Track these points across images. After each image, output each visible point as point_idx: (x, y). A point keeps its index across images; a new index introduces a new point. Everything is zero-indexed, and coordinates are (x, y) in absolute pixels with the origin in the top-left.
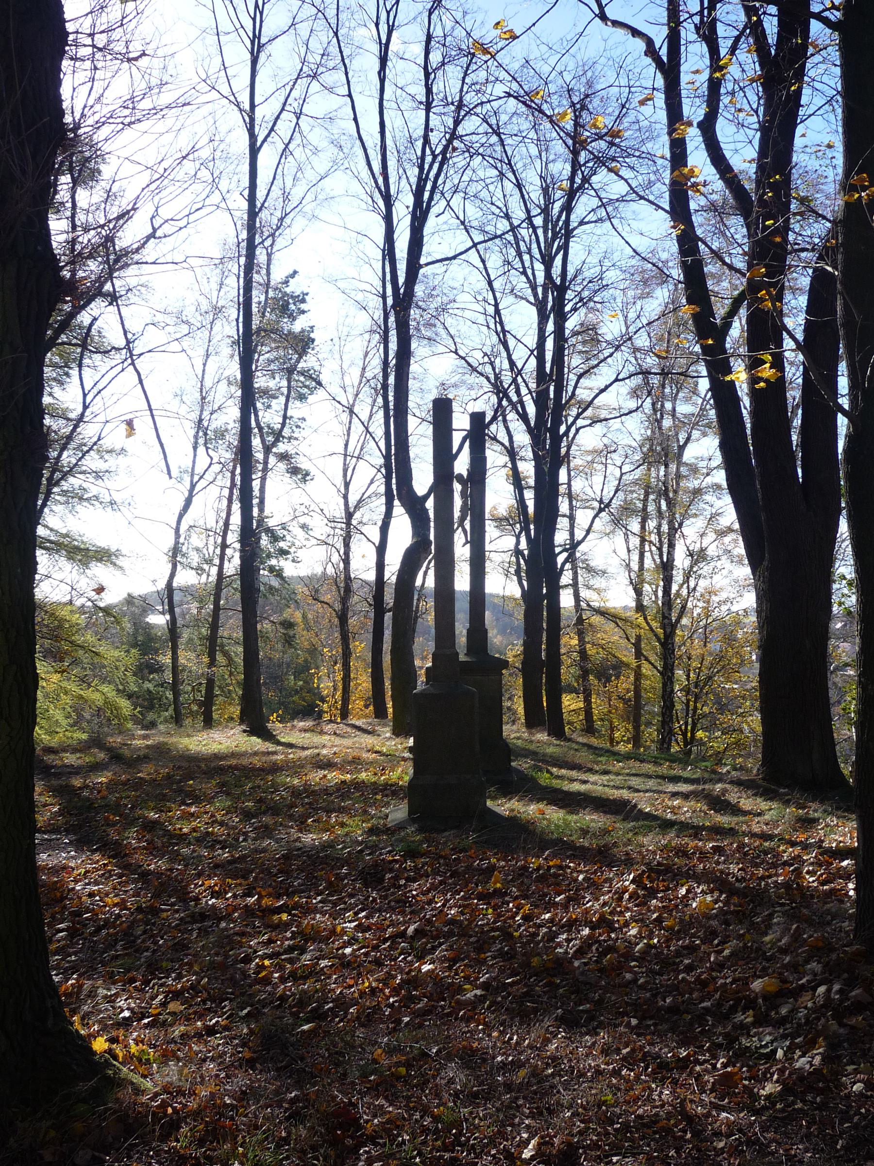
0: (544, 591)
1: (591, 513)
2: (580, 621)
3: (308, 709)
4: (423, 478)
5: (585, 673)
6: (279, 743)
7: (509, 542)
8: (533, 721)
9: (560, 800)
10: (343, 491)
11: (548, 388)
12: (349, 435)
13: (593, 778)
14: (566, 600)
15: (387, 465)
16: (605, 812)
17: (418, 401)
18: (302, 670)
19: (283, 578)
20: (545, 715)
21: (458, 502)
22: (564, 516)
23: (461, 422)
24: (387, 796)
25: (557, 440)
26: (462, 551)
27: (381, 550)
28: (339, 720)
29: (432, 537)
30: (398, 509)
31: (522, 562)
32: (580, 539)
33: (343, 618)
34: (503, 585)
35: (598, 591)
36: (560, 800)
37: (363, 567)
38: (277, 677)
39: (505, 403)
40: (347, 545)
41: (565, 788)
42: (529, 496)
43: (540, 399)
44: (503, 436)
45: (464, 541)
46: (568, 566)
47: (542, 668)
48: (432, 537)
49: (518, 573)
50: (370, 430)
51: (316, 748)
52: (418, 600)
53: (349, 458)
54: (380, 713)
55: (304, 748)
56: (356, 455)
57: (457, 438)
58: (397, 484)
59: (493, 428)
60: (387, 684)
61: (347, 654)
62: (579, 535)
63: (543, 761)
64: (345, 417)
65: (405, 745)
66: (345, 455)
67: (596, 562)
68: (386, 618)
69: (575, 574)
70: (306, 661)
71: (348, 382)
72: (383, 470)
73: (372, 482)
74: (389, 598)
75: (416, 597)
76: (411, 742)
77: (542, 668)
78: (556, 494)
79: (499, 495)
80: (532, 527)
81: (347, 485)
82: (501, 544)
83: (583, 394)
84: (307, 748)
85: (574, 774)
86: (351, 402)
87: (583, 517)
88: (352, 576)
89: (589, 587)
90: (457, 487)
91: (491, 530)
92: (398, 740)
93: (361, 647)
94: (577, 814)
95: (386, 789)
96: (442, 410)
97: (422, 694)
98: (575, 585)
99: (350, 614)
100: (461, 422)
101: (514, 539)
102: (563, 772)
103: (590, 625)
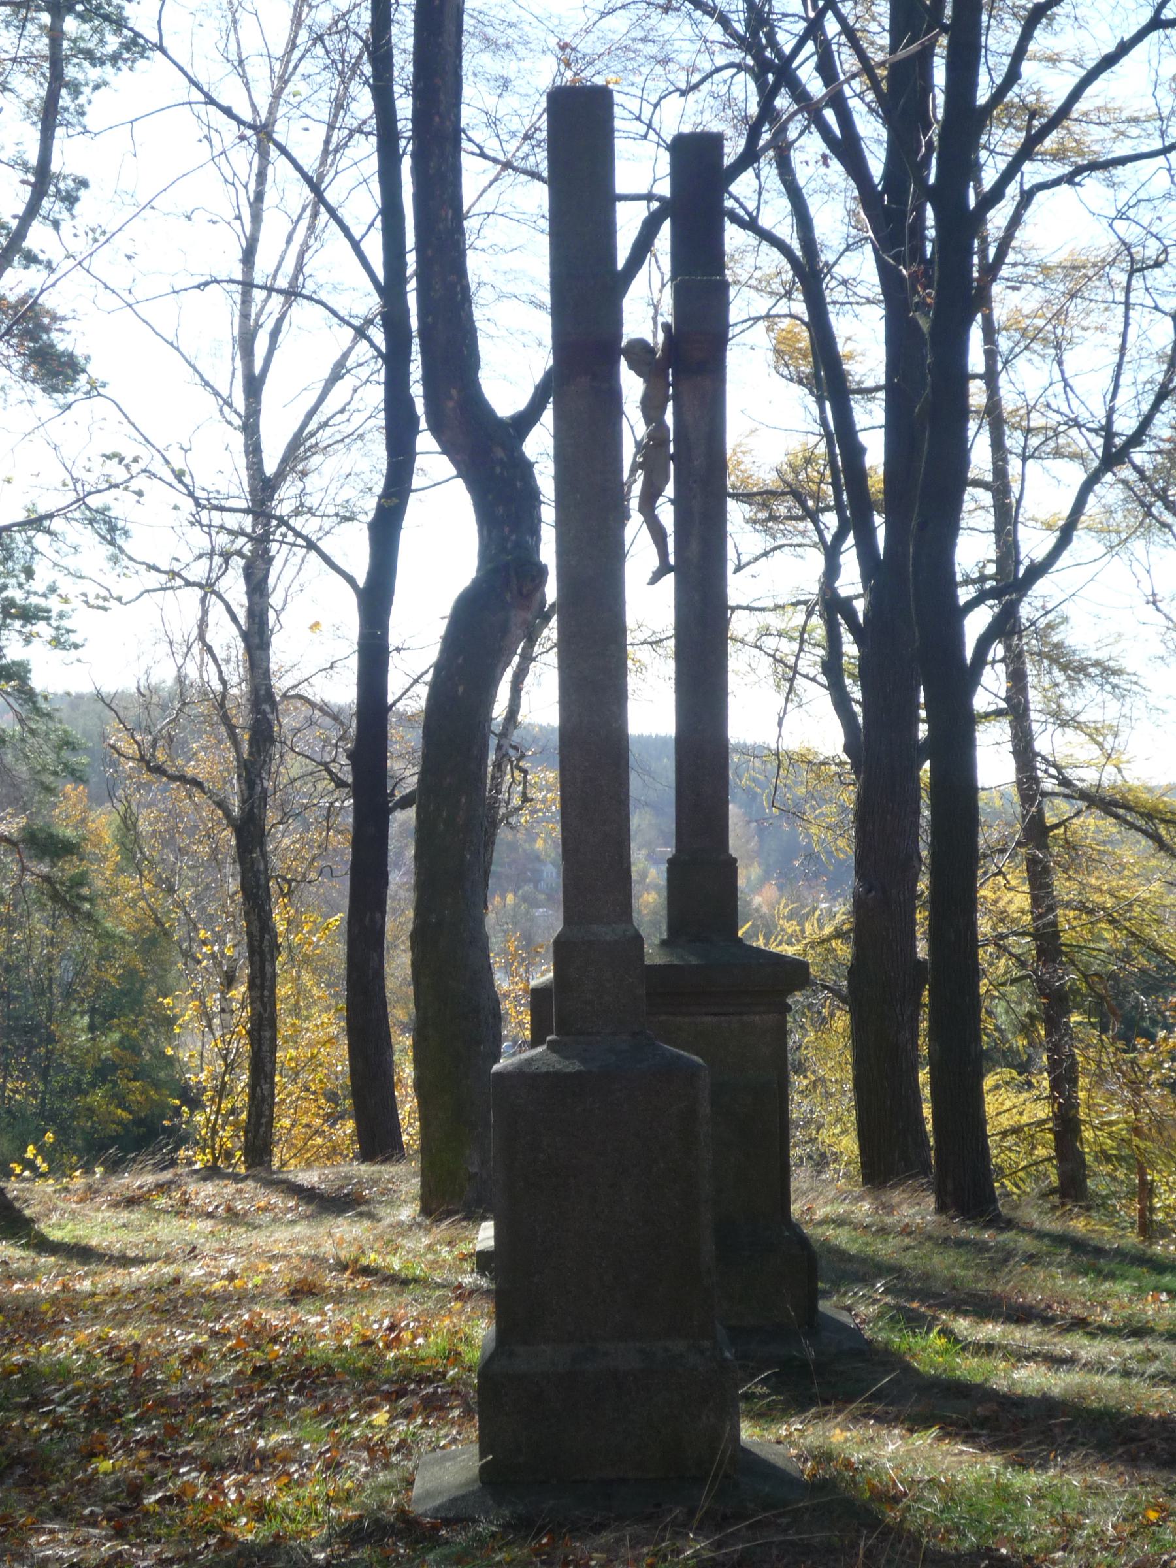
0: (923, 730)
1: (1076, 475)
2: (1036, 831)
3: (134, 1131)
4: (514, 357)
5: (1055, 1004)
6: (44, 1245)
7: (801, 571)
8: (886, 1157)
9: (983, 1422)
10: (240, 402)
11: (926, 56)
12: (257, 218)
13: (1090, 1349)
14: (993, 764)
15: (393, 318)
16: (1133, 1461)
17: (490, 102)
18: (127, 1002)
19: (27, 695)
20: (924, 1141)
21: (633, 427)
22: (977, 483)
23: (640, 170)
24: (408, 1414)
25: (962, 226)
26: (649, 605)
27: (375, 599)
28: (242, 1170)
29: (548, 553)
30: (432, 461)
31: (847, 638)
32: (1039, 555)
33: (250, 832)
34: (789, 718)
35: (1094, 733)
36: (983, 1422)
37: (316, 658)
38: (34, 1029)
39: (783, 102)
40: (257, 586)
41: (999, 1384)
42: (870, 420)
43: (901, 97)
44: (776, 215)
45: (654, 563)
46: (998, 650)
47: (915, 984)
48: (548, 553)
49: (832, 667)
50: (330, 196)
51: (169, 1259)
52: (498, 766)
53: (258, 295)
54: (378, 1140)
55: (124, 1261)
56: (283, 283)
57: (628, 221)
58: (427, 380)
59: (743, 187)
60: (403, 1043)
61: (262, 946)
62: (1033, 544)
63: (924, 1295)
64: (243, 159)
65: (465, 1248)
66: (248, 285)
67: (1079, 638)
68: (394, 829)
69: (1017, 678)
70: (130, 973)
71: (251, 43)
72: (378, 335)
73: (336, 375)
74: (404, 769)
75: (492, 757)
76: (485, 1235)
77: (915, 984)
78: (956, 411)
79: (767, 419)
80: (879, 520)
81: (254, 386)
82: (776, 575)
83: (1045, 83)
84: (140, 1261)
85: (1028, 1336)
86: (264, 115)
87: (1046, 489)
88: (280, 685)
89: (1064, 720)
90: (632, 386)
91: (741, 530)
92: (442, 1230)
93: (315, 929)
94: (1044, 1467)
95: (401, 1393)
96: (579, 124)
97: (521, 1076)
98: (1016, 710)
99: (272, 816)
100: (640, 170)
101: (816, 561)
102: (991, 1331)
103: (1069, 846)
